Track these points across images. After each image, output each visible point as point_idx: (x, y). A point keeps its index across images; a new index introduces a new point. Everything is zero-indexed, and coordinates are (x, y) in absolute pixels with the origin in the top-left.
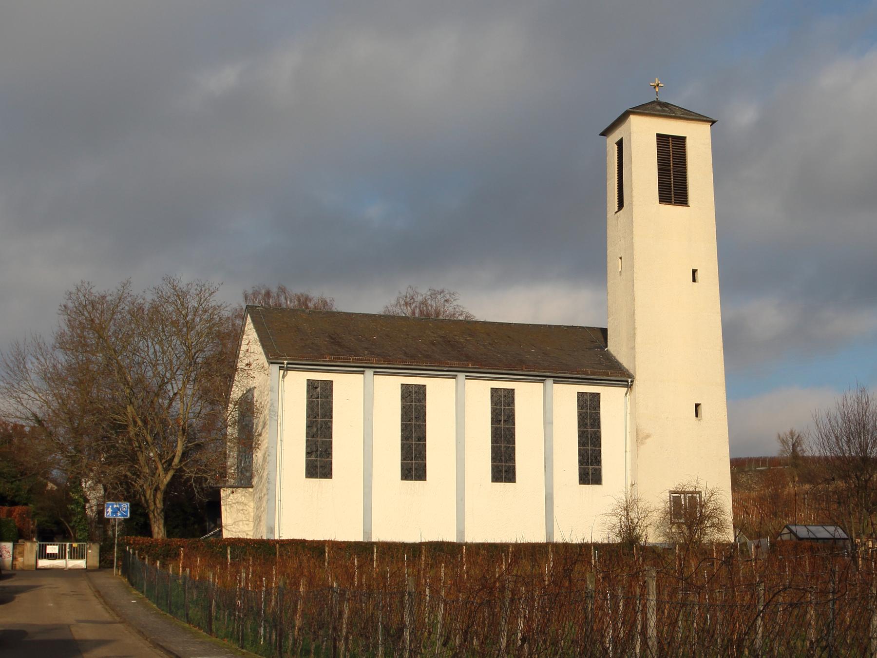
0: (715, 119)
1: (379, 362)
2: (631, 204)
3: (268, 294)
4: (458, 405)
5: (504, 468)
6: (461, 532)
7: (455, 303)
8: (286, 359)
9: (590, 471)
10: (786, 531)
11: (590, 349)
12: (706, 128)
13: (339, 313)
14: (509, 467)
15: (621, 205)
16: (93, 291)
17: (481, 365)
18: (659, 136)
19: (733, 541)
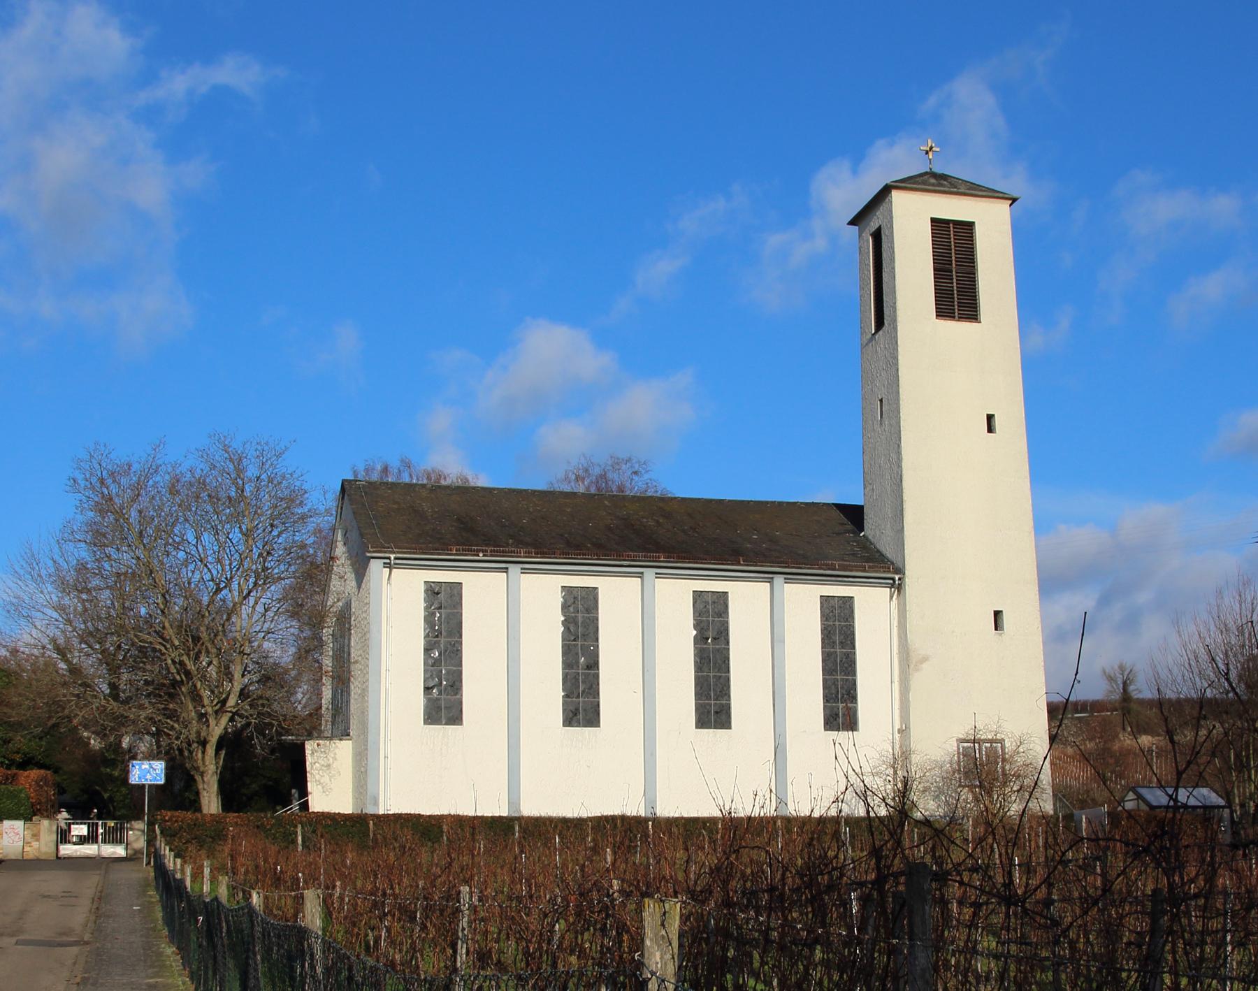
0: (1015, 196)
1: (528, 555)
2: (894, 321)
3: (385, 470)
4: (645, 611)
5: (713, 708)
6: (650, 799)
7: (646, 477)
8: (393, 552)
9: (840, 710)
10: (1131, 796)
11: (838, 534)
12: (1004, 206)
13: (474, 488)
14: (722, 705)
15: (880, 323)
16: (113, 456)
17: (678, 557)
18: (934, 221)
19: (1052, 812)
